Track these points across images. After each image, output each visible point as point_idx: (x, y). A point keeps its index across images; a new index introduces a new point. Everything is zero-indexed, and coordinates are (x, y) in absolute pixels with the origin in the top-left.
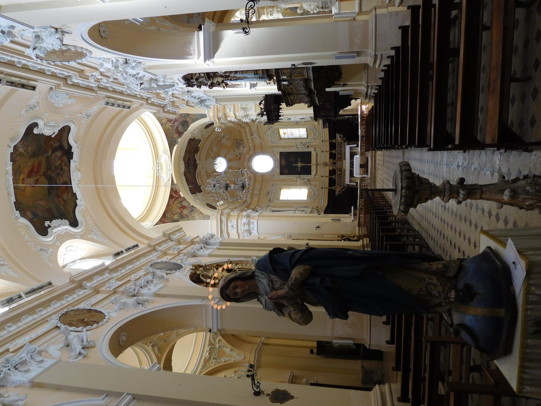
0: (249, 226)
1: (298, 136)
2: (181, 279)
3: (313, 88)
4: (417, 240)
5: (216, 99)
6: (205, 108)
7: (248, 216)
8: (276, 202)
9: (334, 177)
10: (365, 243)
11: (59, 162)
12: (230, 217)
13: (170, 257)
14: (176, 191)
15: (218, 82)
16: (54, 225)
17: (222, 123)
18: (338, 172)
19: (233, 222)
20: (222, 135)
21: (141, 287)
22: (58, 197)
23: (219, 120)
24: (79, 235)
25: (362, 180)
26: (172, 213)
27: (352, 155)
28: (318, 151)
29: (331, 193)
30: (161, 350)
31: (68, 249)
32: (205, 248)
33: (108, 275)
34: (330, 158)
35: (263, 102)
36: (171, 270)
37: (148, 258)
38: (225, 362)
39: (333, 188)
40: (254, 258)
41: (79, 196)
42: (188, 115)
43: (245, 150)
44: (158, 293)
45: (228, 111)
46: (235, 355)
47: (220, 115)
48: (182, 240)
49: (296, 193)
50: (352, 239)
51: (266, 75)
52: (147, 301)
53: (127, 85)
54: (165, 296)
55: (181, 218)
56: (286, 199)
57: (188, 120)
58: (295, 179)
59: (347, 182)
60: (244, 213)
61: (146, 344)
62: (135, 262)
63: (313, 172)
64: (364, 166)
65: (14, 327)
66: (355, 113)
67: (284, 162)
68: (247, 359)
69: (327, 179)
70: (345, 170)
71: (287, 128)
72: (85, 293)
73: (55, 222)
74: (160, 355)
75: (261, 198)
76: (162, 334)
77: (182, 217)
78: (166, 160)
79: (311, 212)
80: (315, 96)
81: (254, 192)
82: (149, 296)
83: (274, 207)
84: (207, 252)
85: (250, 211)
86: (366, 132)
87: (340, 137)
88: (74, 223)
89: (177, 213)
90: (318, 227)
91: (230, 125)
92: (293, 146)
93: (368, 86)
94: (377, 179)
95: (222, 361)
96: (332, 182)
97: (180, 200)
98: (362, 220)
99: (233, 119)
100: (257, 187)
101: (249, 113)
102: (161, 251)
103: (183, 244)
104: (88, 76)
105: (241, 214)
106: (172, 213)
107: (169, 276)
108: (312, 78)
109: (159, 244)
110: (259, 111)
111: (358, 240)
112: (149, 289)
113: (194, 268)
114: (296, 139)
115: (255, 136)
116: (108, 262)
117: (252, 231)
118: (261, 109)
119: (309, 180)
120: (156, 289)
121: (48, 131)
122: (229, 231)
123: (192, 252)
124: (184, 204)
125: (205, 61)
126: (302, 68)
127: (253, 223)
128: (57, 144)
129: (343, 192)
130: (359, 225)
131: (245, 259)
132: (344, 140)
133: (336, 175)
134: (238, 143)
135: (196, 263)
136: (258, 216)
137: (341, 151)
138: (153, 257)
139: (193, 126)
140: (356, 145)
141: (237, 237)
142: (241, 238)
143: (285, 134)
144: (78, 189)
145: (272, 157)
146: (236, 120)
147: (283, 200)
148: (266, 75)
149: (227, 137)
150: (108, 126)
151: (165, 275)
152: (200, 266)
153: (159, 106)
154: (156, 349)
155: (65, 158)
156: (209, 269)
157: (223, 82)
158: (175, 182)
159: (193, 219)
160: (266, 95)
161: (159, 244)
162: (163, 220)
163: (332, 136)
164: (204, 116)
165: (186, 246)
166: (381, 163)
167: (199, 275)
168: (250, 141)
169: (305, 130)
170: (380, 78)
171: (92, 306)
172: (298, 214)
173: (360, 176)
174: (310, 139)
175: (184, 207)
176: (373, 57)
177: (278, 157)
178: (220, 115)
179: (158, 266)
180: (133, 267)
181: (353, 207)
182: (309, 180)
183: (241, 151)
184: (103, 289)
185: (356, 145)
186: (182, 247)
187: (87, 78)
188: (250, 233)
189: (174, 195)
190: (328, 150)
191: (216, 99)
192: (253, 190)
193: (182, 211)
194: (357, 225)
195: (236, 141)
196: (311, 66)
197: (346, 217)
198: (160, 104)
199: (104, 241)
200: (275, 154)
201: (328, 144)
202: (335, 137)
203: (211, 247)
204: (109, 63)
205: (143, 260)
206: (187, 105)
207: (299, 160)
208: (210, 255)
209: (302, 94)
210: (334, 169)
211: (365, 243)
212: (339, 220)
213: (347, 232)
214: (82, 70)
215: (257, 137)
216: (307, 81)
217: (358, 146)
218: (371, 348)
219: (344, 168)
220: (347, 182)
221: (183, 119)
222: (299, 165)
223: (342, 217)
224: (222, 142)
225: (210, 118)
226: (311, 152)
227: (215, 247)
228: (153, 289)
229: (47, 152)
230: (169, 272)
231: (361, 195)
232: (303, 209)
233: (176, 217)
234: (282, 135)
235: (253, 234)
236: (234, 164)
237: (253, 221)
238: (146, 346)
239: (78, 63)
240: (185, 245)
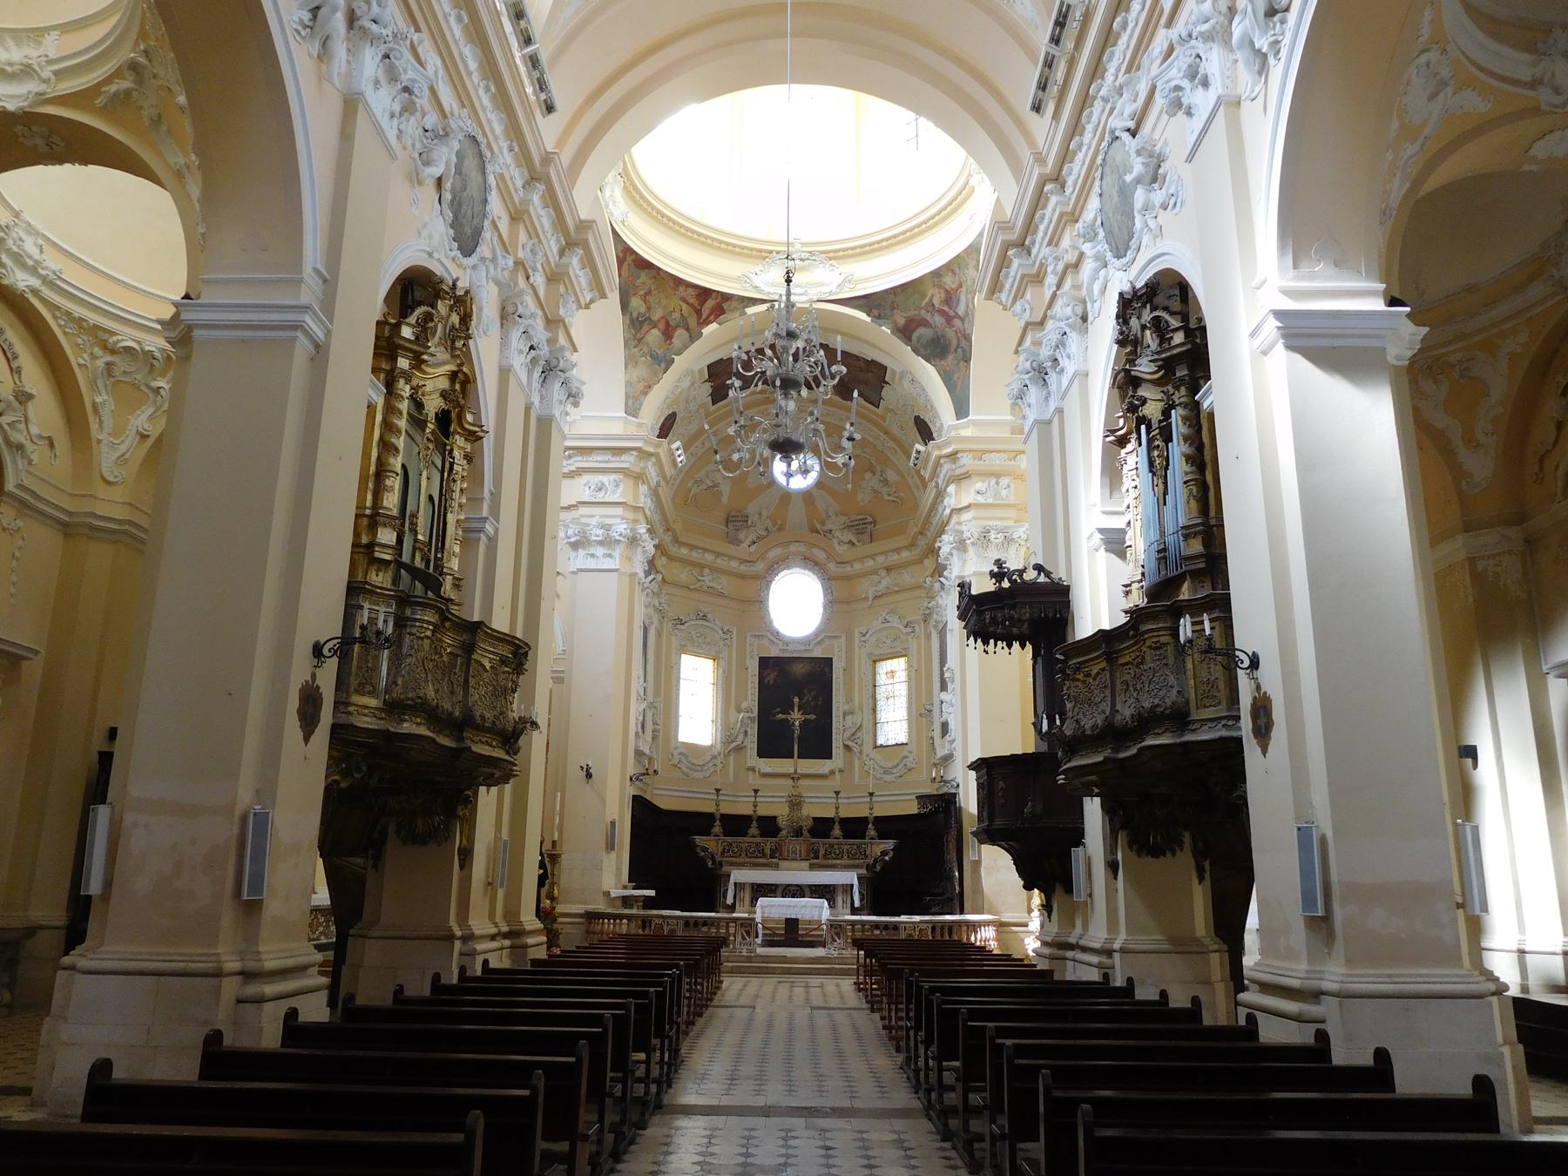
1: (882, 716)
2: (420, 239)
5: (1049, 422)
6: (1016, 386)
7: (633, 541)
8: (675, 643)
9: (754, 830)
10: (531, 941)
12: (631, 482)
13: (504, 225)
15: (1144, 401)
17: (937, 464)
18: (769, 844)
19: (617, 490)
20: (892, 476)
21: (387, 56)
23: (948, 456)
25: (748, 926)
26: (649, 292)
27: (825, 892)
28: (836, 782)
29: (700, 822)
30: (119, 105)
32: (534, 361)
35: (1042, 579)
36: (457, 205)
37: (504, 145)
38: (95, 405)
39: (717, 829)
40: (489, 528)
43: (841, 549)
44: (361, 113)
45: (979, 485)
46: (123, 448)
47: (966, 461)
48: (562, 289)
49: (700, 706)
50: (544, 891)
52: (325, 54)
53: (1128, 83)
54: (346, 135)
55: (632, 321)
56: (682, 675)
58: (744, 705)
59: (739, 875)
60: (642, 529)
61: (143, 35)
62: (487, 90)
63: (768, 765)
64: (791, 933)
66: (967, 905)
67: (799, 670)
68: (102, 492)
69: (746, 810)
70: (776, 867)
71: (909, 681)
74: (99, 102)
76: (182, 99)
77: (636, 325)
78: (821, 284)
80: (1107, 753)
81: (707, 571)
82: (349, 75)
83: (659, 635)
84: (519, 362)
85: (651, 550)
86: (910, 941)
87: (884, 853)
89: (649, 309)
90: (589, 776)
91: (928, 498)
92: (849, 700)
94: (755, 982)
95: (98, 397)
96: (736, 825)
97: (693, 322)
98: (609, 926)
99: (950, 502)
101: (971, 551)
102: (526, 201)
103: (547, 290)
105: (641, 517)
106: (649, 292)
108: (1189, 737)
109: (551, 201)
110: (1013, 564)
111: (539, 913)
112: (377, 82)
113: (460, 293)
114: (874, 710)
115: (886, 582)
117: (581, 552)
118: (1021, 572)
119: (739, 749)
120: (378, 112)
122: (586, 477)
123: (520, 310)
124: (680, 335)
125: (1278, 314)
126: (1234, 699)
127: (610, 556)
129: (703, 861)
130: (591, 916)
131: (486, 494)
132: (874, 865)
133: (759, 839)
134: (864, 527)
135: (480, 309)
136: (633, 575)
137: (839, 856)
138: (503, 162)
139: (928, 375)
140: (857, 904)
141: (564, 503)
142: (564, 516)
145: (817, 633)
146: (947, 511)
147: (678, 663)
150: (959, 61)
151: (437, 171)
152: (466, 319)
153: (1030, 226)
154: (125, 84)
156: (453, 348)
157: (1142, 420)
158: (750, 310)
159: (630, 361)
160: (1067, 589)
161: (551, 201)
162: (629, 259)
163: (888, 826)
164: (961, 410)
165: (542, 294)
166: (816, 998)
167: (433, 306)
168: (870, 563)
169: (903, 738)
170: (1163, 994)
173: (758, 920)
174: (874, 754)
175: (668, 333)
178: (966, 461)
179: (471, 164)
180: (470, 74)
181: (651, 893)
182: (739, 749)
183: (838, 534)
185: (857, 904)
186: (539, 280)
188: (575, 546)
189: (711, 304)
190: (844, 814)
191: (1049, 422)
194: (591, 907)
195: (876, 523)
196: (1246, 723)
197: (619, 869)
198: (1035, 232)
200: (827, 643)
201: (862, 812)
202: (883, 835)
203: (536, 385)
205: (495, 123)
206: (1027, 324)
208: (505, 372)
209: (1113, 706)
211: (531, 941)
212: (610, 846)
213: (569, 874)
215: (882, 586)
216: (1179, 718)
217: (854, 911)
218: (61, 976)
219: (783, 864)
220: (739, 875)
221: (954, 342)
222: (796, 717)
223: (619, 858)
224: (868, 475)
226: (829, 756)
227: (536, 399)
228: (381, 101)
230: (448, 196)
231: (697, 923)
232: (649, 727)
233: (636, 303)
234: (884, 667)
235: (572, 554)
236: (797, 514)
237: (617, 554)
238: (133, 34)
240: (546, 297)
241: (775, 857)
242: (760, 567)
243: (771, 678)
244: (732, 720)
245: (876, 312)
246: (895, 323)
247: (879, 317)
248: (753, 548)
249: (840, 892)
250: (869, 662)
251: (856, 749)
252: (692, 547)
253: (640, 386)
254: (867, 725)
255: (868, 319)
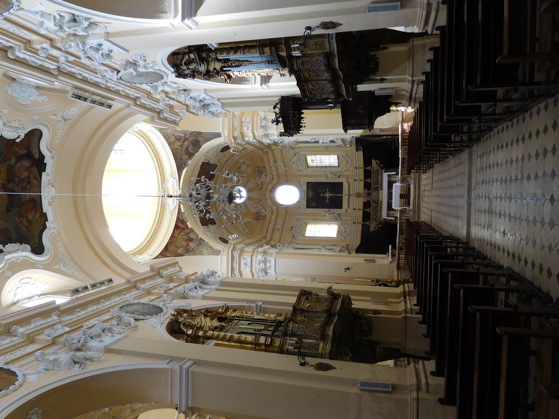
0: (265, 264)
2: (156, 328)
3: (337, 67)
4: (513, 283)
5: (222, 103)
7: (265, 253)
8: (301, 238)
9: (368, 210)
10: (407, 289)
11: (26, 174)
12: (244, 253)
13: (152, 297)
14: (183, 220)
15: (215, 69)
16: (9, 250)
17: (238, 144)
18: (373, 205)
19: (247, 258)
20: (242, 160)
21: (92, 338)
22: (21, 216)
24: (42, 265)
25: (402, 212)
26: (176, 247)
31: (23, 281)
32: (200, 287)
33: (56, 318)
34: (364, 188)
35: (278, 106)
36: (145, 314)
37: (123, 297)
39: (367, 223)
40: (260, 304)
41: (50, 216)
42: (200, 133)
45: (245, 129)
47: (236, 134)
48: (175, 277)
49: (324, 229)
50: (389, 284)
51: (276, 51)
52: (91, 359)
54: (119, 352)
55: (187, 252)
57: (200, 139)
58: (323, 214)
59: (384, 215)
60: (261, 250)
63: (345, 205)
64: (405, 196)
65: (83, 312)
66: (395, 133)
67: (311, 194)
69: (361, 213)
70: (381, 202)
71: (315, 154)
72: (11, 342)
73: (9, 247)
75: (283, 235)
76: (107, 409)
77: (188, 251)
78: (173, 185)
79: (340, 251)
80: (341, 82)
81: (275, 227)
83: (298, 244)
84: (201, 293)
85: (268, 247)
87: (377, 163)
88: (38, 249)
89: (182, 247)
90: (348, 269)
93: (413, 82)
96: (366, 217)
97: (187, 231)
98: (402, 262)
100: (280, 221)
101: (269, 132)
102: (144, 289)
104: (38, 50)
105: (256, 250)
106: (176, 247)
107: (140, 323)
108: (336, 52)
109: (143, 280)
110: (273, 117)
111: (397, 286)
112: (101, 341)
114: (326, 167)
115: (280, 163)
116: (60, 300)
117: (269, 271)
118: (276, 114)
119: (339, 215)
121: (9, 133)
122: (242, 269)
123: (182, 292)
124: (191, 235)
126: (322, 36)
127: (270, 261)
128: (23, 152)
130: (398, 268)
134: (260, 171)
135: (181, 306)
136: (277, 253)
138: (129, 297)
139: (206, 147)
140: (395, 173)
141: (251, 277)
142: (256, 277)
143: (312, 161)
144: (50, 208)
146: (255, 140)
148: (276, 51)
149: (247, 163)
150: (93, 135)
151: (132, 321)
152: (185, 311)
155: (35, 170)
156: (196, 316)
157: (221, 69)
158: (183, 211)
159: (201, 253)
160: (282, 97)
161: (143, 280)
162: (164, 253)
163: (367, 162)
164: (218, 135)
165: (176, 284)
167: (180, 323)
168: (273, 168)
169: (336, 157)
171: (5, 364)
172: (324, 252)
173: (400, 208)
174: (341, 167)
175: (191, 240)
176: (425, 8)
177: (305, 187)
179: (130, 309)
180: (98, 309)
181: (390, 246)
182: (339, 215)
183: (262, 180)
184: (40, 337)
185: (395, 173)
186: (171, 285)
187: (35, 52)
188: (266, 273)
189: (180, 225)
190: (362, 178)
191: (222, 103)
192: (275, 224)
193: (188, 245)
194: (395, 268)
197: (382, 258)
199: (76, 273)
202: (370, 164)
203: (209, 287)
204: (50, 20)
206: (187, 111)
207: (328, 189)
208: (204, 298)
210: (368, 201)
211: (407, 289)
212: (373, 261)
213: (383, 276)
214: (30, 41)
215: (282, 164)
216: (329, 56)
217: (397, 174)
219: (380, 200)
220: (384, 215)
221: (194, 137)
222: (328, 195)
223: (378, 258)
224: (242, 169)
225: (225, 138)
226: (342, 183)
227: (214, 287)
228: (107, 340)
229: (9, 160)
230: (141, 317)
231: (401, 230)
232: (331, 247)
233: (180, 251)
234: (310, 163)
235: (269, 274)
236: (255, 194)
237: (269, 259)
239: (6, 19)
241: (378, 203)
242: (274, 208)
243: (314, 204)
244: (329, 218)
245: (183, 166)
246: (187, 159)
247: (185, 164)
248: (267, 210)
249: (391, 179)
250: (308, 169)
251: (339, 174)
252: (267, 232)
253: (210, 250)
254: (331, 169)
255: (186, 168)
